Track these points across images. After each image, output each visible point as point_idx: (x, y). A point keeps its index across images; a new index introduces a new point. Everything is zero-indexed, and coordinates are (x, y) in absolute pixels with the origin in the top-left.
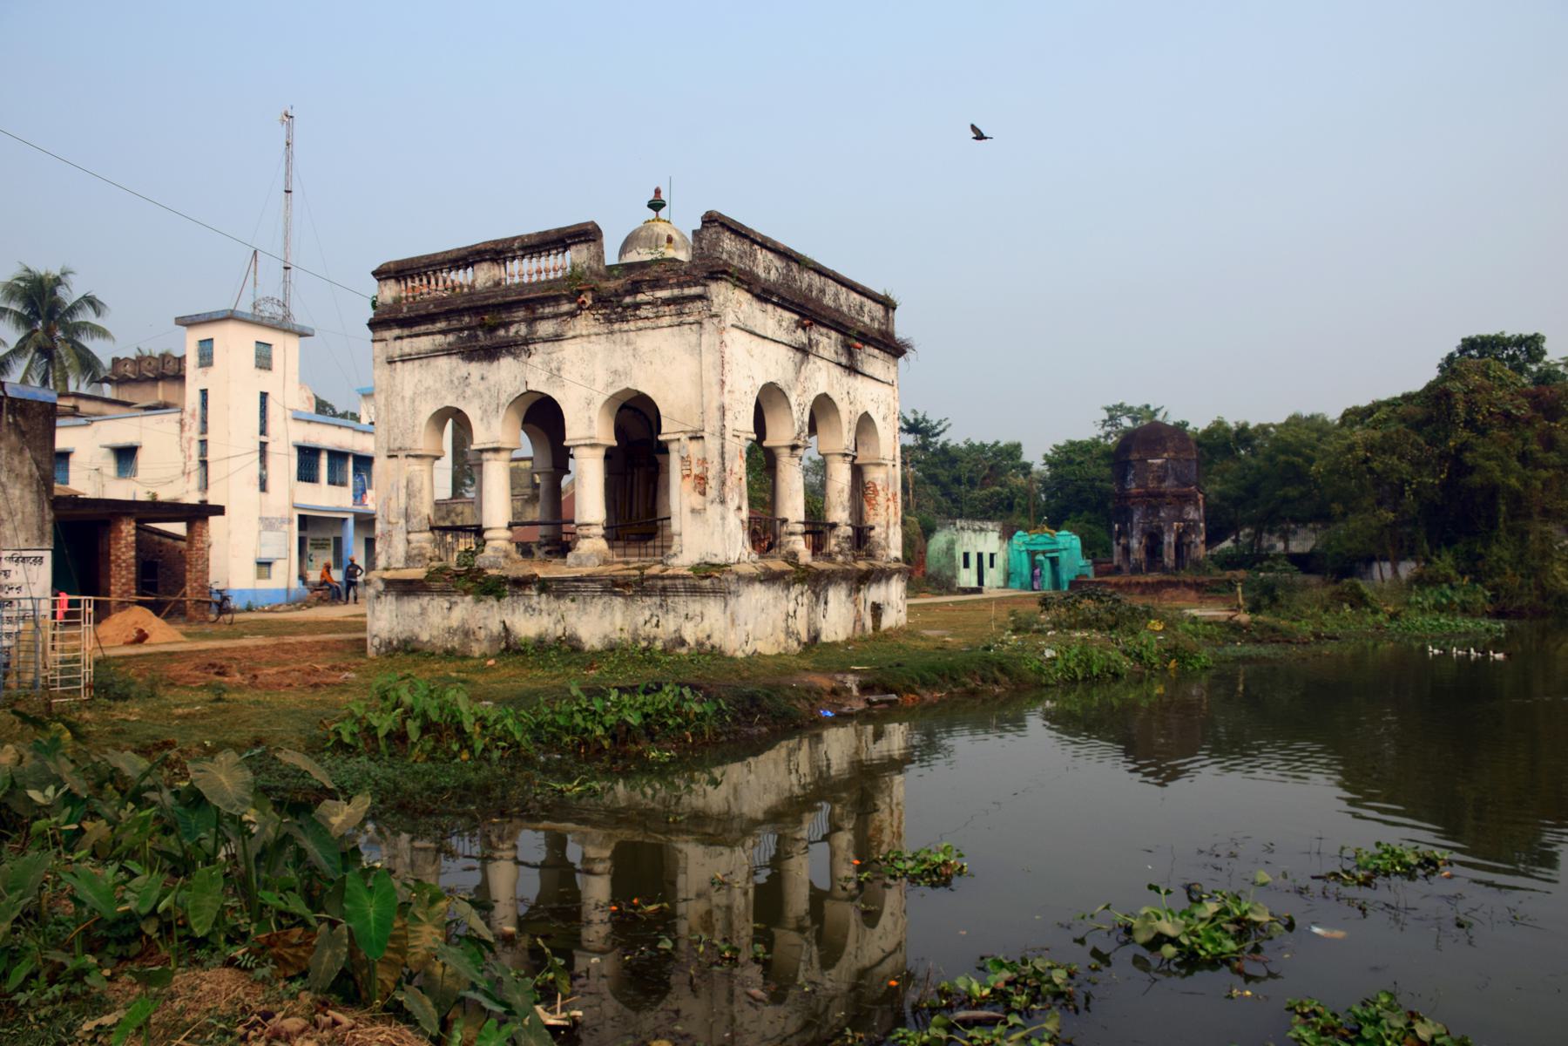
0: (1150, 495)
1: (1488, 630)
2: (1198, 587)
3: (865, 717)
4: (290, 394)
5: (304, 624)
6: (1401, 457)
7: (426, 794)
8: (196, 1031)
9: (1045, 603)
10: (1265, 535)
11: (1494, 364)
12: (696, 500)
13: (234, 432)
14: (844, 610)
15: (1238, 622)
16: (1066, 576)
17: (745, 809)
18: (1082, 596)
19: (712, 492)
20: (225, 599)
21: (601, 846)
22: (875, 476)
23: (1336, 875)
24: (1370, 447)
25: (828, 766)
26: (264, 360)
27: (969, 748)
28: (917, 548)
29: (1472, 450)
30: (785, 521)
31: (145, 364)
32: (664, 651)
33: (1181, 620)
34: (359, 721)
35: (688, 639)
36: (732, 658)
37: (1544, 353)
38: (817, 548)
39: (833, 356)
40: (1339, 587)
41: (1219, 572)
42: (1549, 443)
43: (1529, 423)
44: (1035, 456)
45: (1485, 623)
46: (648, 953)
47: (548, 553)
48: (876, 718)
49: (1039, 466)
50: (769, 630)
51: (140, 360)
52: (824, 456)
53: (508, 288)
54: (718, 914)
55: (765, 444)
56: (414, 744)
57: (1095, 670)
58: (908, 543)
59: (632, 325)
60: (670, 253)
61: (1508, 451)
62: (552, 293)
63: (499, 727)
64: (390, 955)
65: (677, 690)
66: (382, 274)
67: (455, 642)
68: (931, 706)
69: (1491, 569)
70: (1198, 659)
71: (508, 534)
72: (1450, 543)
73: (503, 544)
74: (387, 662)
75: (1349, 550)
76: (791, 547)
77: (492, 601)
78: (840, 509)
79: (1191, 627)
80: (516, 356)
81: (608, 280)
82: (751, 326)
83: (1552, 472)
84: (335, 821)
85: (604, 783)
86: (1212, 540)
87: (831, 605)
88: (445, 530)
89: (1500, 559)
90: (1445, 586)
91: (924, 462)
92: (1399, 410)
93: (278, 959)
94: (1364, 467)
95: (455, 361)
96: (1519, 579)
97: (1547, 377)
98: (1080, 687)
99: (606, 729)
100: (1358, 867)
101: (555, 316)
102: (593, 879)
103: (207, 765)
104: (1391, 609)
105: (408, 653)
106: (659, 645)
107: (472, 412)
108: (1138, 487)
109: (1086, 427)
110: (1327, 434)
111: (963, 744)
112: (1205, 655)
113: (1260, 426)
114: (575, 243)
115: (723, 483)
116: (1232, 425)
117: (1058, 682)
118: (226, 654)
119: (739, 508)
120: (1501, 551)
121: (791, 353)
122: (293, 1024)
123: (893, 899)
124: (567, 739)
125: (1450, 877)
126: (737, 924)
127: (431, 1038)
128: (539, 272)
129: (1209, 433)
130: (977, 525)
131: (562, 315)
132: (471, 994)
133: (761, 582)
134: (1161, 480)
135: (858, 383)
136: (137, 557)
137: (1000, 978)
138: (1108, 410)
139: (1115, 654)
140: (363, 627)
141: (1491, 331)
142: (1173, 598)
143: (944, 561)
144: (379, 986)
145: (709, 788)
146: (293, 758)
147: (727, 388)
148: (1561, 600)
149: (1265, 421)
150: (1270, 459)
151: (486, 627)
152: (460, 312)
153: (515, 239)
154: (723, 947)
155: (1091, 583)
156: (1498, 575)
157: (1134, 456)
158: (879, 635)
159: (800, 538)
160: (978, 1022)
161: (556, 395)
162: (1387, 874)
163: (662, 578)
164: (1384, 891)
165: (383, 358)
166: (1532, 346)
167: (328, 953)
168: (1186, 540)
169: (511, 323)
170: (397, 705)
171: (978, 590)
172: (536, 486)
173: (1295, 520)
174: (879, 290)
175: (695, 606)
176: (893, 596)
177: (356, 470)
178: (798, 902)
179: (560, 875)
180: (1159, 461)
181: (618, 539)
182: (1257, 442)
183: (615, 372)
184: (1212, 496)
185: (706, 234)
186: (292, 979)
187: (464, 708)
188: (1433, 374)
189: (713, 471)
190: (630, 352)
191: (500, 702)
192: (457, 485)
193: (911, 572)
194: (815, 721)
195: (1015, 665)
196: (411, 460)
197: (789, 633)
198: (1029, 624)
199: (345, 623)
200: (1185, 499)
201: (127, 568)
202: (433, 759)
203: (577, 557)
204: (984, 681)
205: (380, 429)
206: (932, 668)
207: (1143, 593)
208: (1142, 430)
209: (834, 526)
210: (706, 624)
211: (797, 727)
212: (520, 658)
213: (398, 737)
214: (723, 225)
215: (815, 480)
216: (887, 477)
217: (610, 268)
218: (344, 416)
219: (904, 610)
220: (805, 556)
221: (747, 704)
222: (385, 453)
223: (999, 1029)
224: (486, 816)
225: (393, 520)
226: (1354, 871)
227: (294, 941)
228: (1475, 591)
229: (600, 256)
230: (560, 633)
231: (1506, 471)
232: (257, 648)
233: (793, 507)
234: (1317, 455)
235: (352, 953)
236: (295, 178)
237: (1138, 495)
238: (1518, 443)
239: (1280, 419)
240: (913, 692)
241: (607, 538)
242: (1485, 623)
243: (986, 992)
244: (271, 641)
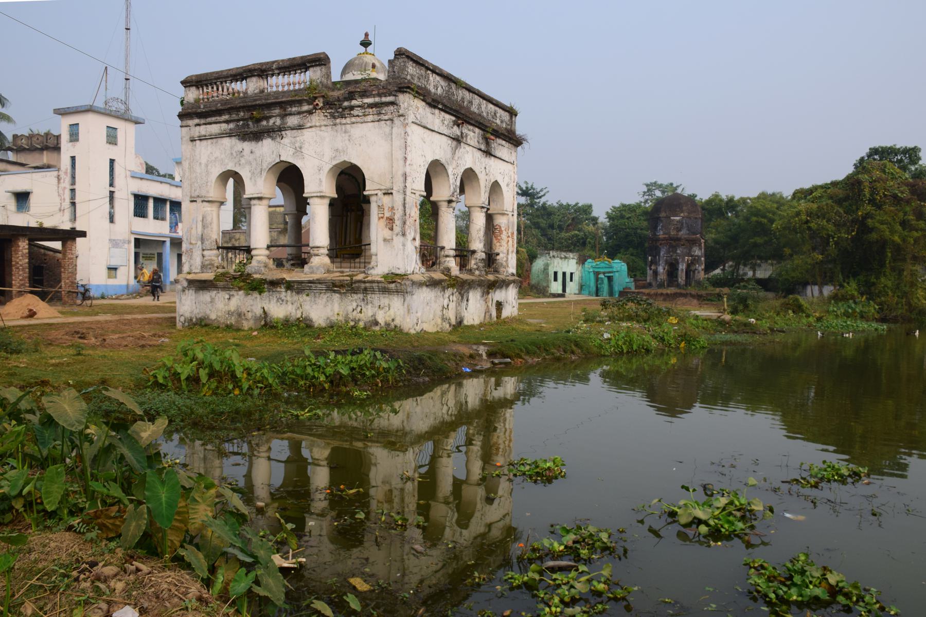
0: (671, 239)
1: (876, 330)
2: (699, 297)
3: (491, 372)
4: (129, 161)
6: (828, 221)
8: (46, 574)
9: (604, 304)
10: (741, 267)
11: (889, 165)
12: (387, 233)
13: (93, 183)
14: (479, 305)
15: (723, 320)
16: (617, 288)
17: (414, 428)
18: (628, 301)
20: (87, 290)
22: (501, 221)
24: (810, 214)
26: (112, 138)
27: (557, 396)
29: (872, 218)
30: (443, 248)
32: (365, 328)
34: (169, 369)
35: (380, 321)
36: (407, 334)
37: (920, 159)
38: (463, 266)
39: (476, 144)
40: (786, 300)
41: (712, 288)
43: (908, 202)
44: (601, 213)
45: (875, 325)
46: (349, 521)
47: (292, 265)
48: (496, 374)
49: (603, 219)
50: (431, 316)
51: (31, 137)
52: (469, 207)
53: (269, 94)
54: (396, 493)
55: (432, 199)
56: (204, 384)
57: (635, 347)
58: (520, 265)
59: (348, 120)
60: (374, 75)
61: (894, 219)
62: (297, 98)
63: (258, 374)
64: (177, 524)
65: (372, 353)
66: (187, 83)
67: (232, 320)
68: (532, 366)
69: (880, 292)
71: (267, 252)
73: (263, 259)
74: (189, 333)
75: (793, 277)
77: (256, 294)
78: (478, 242)
79: (695, 322)
80: (273, 139)
82: (424, 123)
83: (920, 233)
84: (144, 435)
87: (470, 301)
89: (885, 286)
90: (851, 301)
91: (531, 214)
92: (829, 191)
93: (102, 527)
94: (805, 226)
95: (234, 140)
96: (896, 299)
98: (624, 358)
100: (811, 476)
101: (299, 113)
102: (318, 468)
103: (55, 398)
104: (817, 315)
105: (203, 326)
106: (361, 324)
107: (245, 174)
108: (664, 234)
109: (633, 196)
110: (783, 205)
112: (703, 340)
113: (742, 198)
114: (312, 66)
115: (404, 223)
116: (724, 197)
118: (86, 325)
119: (414, 239)
120: (887, 282)
121: (450, 141)
122: (109, 570)
124: (302, 383)
125: (868, 484)
126: (407, 500)
127: (203, 580)
128: (289, 84)
129: (709, 202)
130: (563, 254)
131: (303, 112)
132: (230, 550)
133: (427, 286)
134: (679, 230)
135: (492, 161)
136: (29, 263)
137: (570, 538)
138: (647, 185)
139: (647, 338)
140: (173, 310)
142: (684, 304)
143: (541, 277)
145: (391, 414)
147: (408, 163)
148: (921, 312)
150: (747, 219)
151: (252, 311)
152: (237, 109)
153: (273, 62)
154: (397, 517)
155: (634, 293)
156: (884, 296)
157: (663, 215)
158: (501, 321)
159: (452, 259)
160: (561, 569)
162: (829, 481)
163: (364, 282)
165: (188, 138)
166: (912, 154)
167: (134, 524)
168: (693, 268)
169: (270, 117)
170: (194, 359)
171: (562, 296)
172: (286, 223)
173: (760, 258)
174: (507, 103)
175: (385, 300)
176: (510, 297)
177: (171, 210)
178: (445, 487)
179: (298, 465)
180: (678, 218)
181: (337, 257)
182: (739, 209)
183: (337, 150)
185: (397, 63)
186: (111, 540)
187: (236, 362)
188: (850, 170)
190: (347, 138)
191: (260, 358)
192: (236, 222)
193: (521, 282)
194: (459, 374)
196: (205, 203)
197: (444, 319)
198: (594, 317)
199: (163, 307)
200: (693, 242)
201: (23, 269)
202: (216, 394)
203: (311, 268)
204: (565, 352)
205: (186, 184)
206: (533, 343)
207: (664, 300)
208: (668, 198)
209: (474, 252)
210: (392, 312)
211: (448, 378)
212: (274, 331)
213: (194, 380)
214: (408, 57)
215: (462, 223)
216: (508, 223)
217: (335, 83)
218: (164, 176)
219: (517, 306)
220: (455, 270)
221: (416, 363)
222: (188, 199)
224: (249, 431)
225: (193, 242)
226: (808, 478)
227: (113, 515)
228: (869, 305)
229: (328, 75)
230: (299, 315)
231: (892, 232)
232: (106, 322)
233: (448, 240)
234: (776, 218)
235: (151, 523)
238: (901, 214)
239: (754, 194)
240: (521, 357)
241: (330, 256)
242: (875, 325)
243: (562, 548)
244: (116, 317)
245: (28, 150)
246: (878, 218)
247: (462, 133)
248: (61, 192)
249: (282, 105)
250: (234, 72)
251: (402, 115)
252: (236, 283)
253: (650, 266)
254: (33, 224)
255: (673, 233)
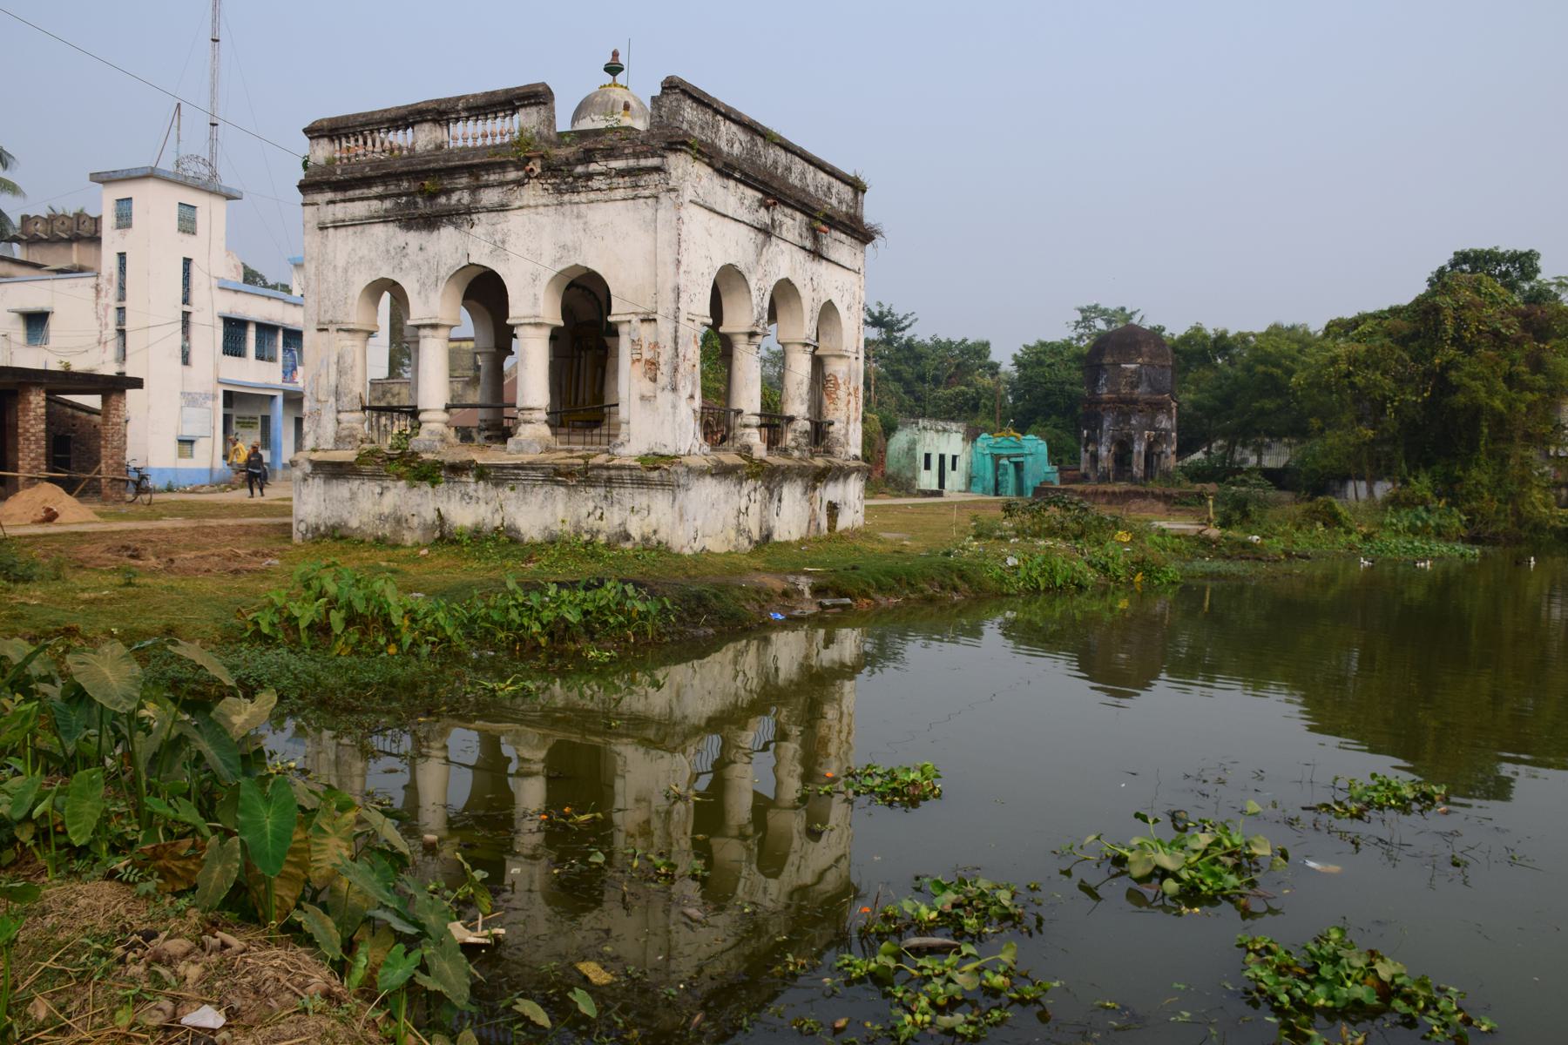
0: (1122, 401)
1: (1462, 555)
2: (1167, 499)
3: (817, 621)
5: (228, 506)
7: (349, 689)
9: (1008, 509)
11: (1487, 280)
12: (646, 387)
13: (154, 299)
14: (798, 509)
15: (1207, 537)
16: (1030, 482)
18: (1048, 503)
19: (663, 379)
21: (537, 747)
22: (836, 368)
23: (1327, 806)
24: (1353, 360)
25: (777, 669)
26: (187, 224)
27: (923, 657)
28: (877, 448)
29: (1457, 369)
30: (739, 412)
31: (58, 223)
32: (608, 545)
33: (1149, 532)
34: (279, 611)
35: (633, 533)
36: (679, 555)
37: (1538, 271)
38: (772, 442)
39: (797, 240)
40: (1313, 504)
42: (1537, 365)
43: (1518, 343)
44: (1004, 356)
46: (578, 866)
47: (488, 438)
48: (827, 623)
49: (1008, 367)
50: (719, 526)
51: (51, 219)
53: (451, 152)
54: (656, 824)
55: (722, 330)
57: (1059, 581)
58: (868, 441)
59: (583, 197)
60: (627, 121)
61: (1494, 372)
62: (497, 159)
63: (429, 620)
64: (290, 869)
65: (620, 586)
66: (314, 132)
67: (387, 530)
70: (1166, 573)
71: (445, 417)
72: (1428, 464)
73: (439, 427)
74: (313, 549)
75: (1324, 467)
76: (745, 440)
77: (426, 487)
79: (1159, 540)
80: (457, 226)
81: (558, 147)
82: (710, 202)
83: (1537, 396)
84: (238, 720)
85: (538, 683)
86: (1182, 452)
88: (379, 410)
89: (1479, 483)
90: (1421, 508)
91: (888, 358)
92: (1386, 323)
93: (165, 873)
94: (1346, 382)
95: (392, 229)
96: (1496, 505)
97: (1540, 296)
98: (1042, 598)
99: (543, 626)
100: (1351, 799)
101: (501, 184)
103: (90, 657)
104: (1365, 530)
105: (336, 540)
106: (602, 539)
109: (1059, 328)
110: (1309, 345)
111: (917, 651)
113: (1240, 334)
115: (676, 370)
117: (1020, 592)
119: (692, 397)
120: (1480, 475)
121: (752, 234)
122: (177, 946)
123: (838, 812)
124: (501, 635)
125: (1447, 813)
127: (333, 963)
128: (485, 136)
129: (1186, 339)
130: (941, 425)
131: (508, 183)
132: (380, 914)
134: (1134, 386)
136: (47, 430)
138: (1082, 311)
139: (1080, 565)
140: (288, 512)
141: (1486, 246)
142: (1140, 509)
143: (904, 461)
144: (277, 902)
145: (651, 690)
146: (189, 651)
149: (1246, 330)
150: (1248, 369)
151: (419, 515)
152: (397, 176)
153: (459, 99)
154: (659, 862)
155: (1058, 490)
156: (1475, 499)
157: (1107, 360)
159: (755, 431)
160: (931, 950)
161: (500, 270)
162: (1381, 807)
163: (608, 468)
164: (1375, 826)
166: (1525, 262)
167: (218, 868)
168: (1157, 450)
169: (453, 190)
170: (321, 595)
171: (938, 494)
172: (478, 368)
173: (1270, 434)
174: (849, 171)
175: (641, 498)
176: (850, 495)
177: (286, 344)
178: (740, 807)
180: (1133, 366)
181: (562, 425)
182: (1235, 351)
183: (564, 247)
184: (1186, 406)
185: (666, 101)
186: (179, 895)
187: (392, 600)
188: (1422, 288)
189: (665, 356)
190: (581, 226)
192: (394, 365)
193: (870, 471)
195: (975, 572)
196: (342, 334)
200: (1158, 407)
203: (519, 443)
204: (942, 588)
205: (310, 301)
206: (888, 573)
207: (1109, 503)
209: (791, 419)
211: (746, 629)
212: (455, 549)
213: (321, 629)
214: (684, 92)
215: (772, 372)
216: (849, 371)
218: (275, 287)
219: (862, 511)
220: (760, 450)
221: (693, 604)
222: (314, 326)
223: (952, 959)
224: (412, 715)
225: (322, 398)
226: (1347, 803)
227: (183, 853)
228: (1450, 514)
229: (551, 121)
230: (498, 523)
231: (1491, 392)
232: (175, 530)
233: (748, 398)
234: (1298, 367)
235: (247, 867)
236: (223, 27)
237: (1110, 401)
238: (1506, 363)
239: (1260, 328)
240: (868, 596)
242: (1460, 547)
244: (191, 523)
245: (46, 241)
246: (1467, 368)
247: (773, 220)
248: (101, 312)
249: (474, 170)
250: (393, 114)
251: (673, 190)
252: (392, 468)
253: (1086, 446)
254: (54, 366)
255: (1124, 391)
